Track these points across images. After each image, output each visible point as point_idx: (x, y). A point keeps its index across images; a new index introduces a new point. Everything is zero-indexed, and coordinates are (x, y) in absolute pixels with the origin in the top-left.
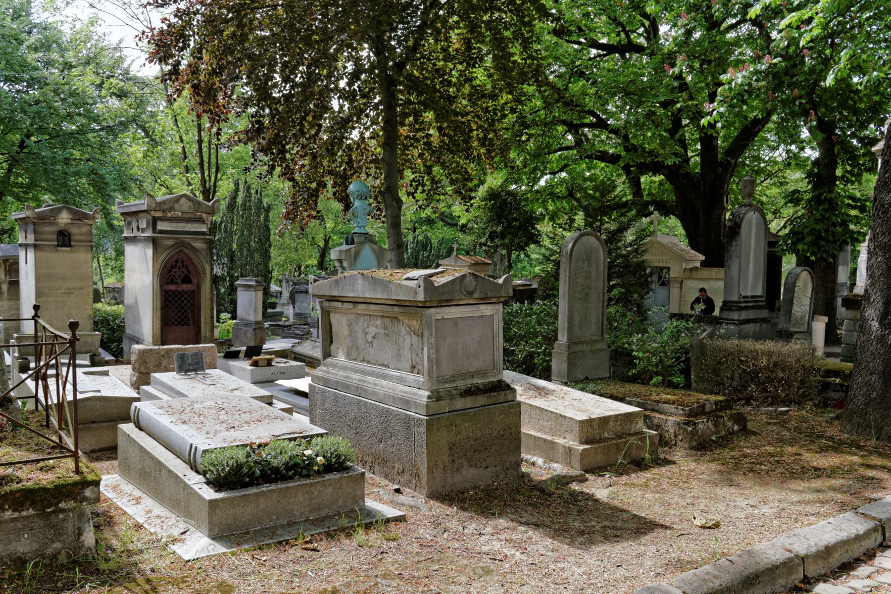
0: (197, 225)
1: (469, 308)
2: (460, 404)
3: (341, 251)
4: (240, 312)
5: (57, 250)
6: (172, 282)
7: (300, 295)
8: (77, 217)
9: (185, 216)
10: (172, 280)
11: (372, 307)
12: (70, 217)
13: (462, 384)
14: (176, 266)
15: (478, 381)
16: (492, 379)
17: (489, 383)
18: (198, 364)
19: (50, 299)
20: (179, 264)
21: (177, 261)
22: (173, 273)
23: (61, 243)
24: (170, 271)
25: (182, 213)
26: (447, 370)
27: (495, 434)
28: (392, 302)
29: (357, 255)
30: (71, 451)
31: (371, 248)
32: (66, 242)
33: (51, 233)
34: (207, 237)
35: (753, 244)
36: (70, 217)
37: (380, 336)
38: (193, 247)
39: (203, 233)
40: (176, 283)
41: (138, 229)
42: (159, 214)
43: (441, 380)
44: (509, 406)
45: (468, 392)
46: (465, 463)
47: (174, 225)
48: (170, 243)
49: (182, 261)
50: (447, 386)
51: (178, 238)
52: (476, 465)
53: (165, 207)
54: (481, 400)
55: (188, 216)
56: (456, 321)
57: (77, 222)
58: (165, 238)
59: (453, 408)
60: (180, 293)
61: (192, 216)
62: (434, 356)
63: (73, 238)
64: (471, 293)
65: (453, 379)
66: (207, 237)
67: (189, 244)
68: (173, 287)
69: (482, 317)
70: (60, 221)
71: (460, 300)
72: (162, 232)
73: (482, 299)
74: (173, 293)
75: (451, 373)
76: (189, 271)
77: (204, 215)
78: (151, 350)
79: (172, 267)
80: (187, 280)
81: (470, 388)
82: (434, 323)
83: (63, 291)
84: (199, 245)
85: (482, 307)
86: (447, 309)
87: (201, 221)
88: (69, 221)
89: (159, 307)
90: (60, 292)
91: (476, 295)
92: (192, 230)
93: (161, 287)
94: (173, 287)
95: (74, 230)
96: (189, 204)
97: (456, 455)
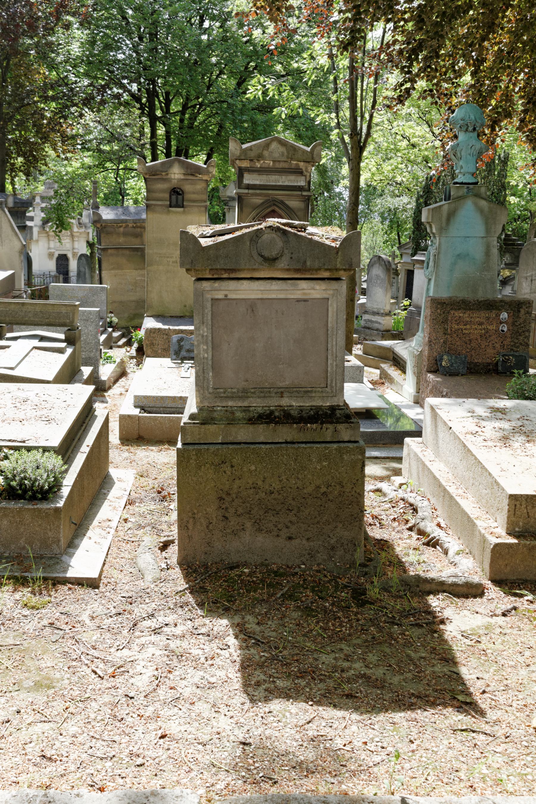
1: (275, 285)
2: (243, 433)
4: (414, 296)
5: (169, 212)
8: (189, 172)
9: (278, 165)
11: (249, 276)
12: (183, 171)
13: (258, 404)
15: (292, 403)
16: (318, 403)
17: (311, 408)
19: (161, 268)
23: (174, 202)
25: (274, 161)
26: (232, 379)
27: (310, 489)
29: (451, 215)
32: (180, 202)
33: (163, 191)
38: (287, 207)
42: (245, 164)
43: (220, 393)
44: (339, 450)
45: (267, 418)
46: (248, 525)
48: (258, 201)
50: (230, 403)
51: (268, 195)
52: (269, 532)
53: (252, 154)
54: (286, 432)
56: (252, 305)
57: (190, 177)
58: (253, 195)
59: (230, 439)
61: (285, 165)
63: (187, 196)
64: (271, 261)
65: (244, 394)
67: (282, 203)
69: (305, 300)
70: (172, 176)
71: (254, 270)
72: (249, 187)
75: (242, 384)
77: (302, 164)
78: (159, 330)
81: (272, 412)
82: (209, 305)
85: (303, 284)
86: (232, 285)
88: (182, 177)
90: (171, 260)
91: (283, 263)
92: (286, 183)
95: (187, 188)
96: (282, 149)
97: (232, 511)
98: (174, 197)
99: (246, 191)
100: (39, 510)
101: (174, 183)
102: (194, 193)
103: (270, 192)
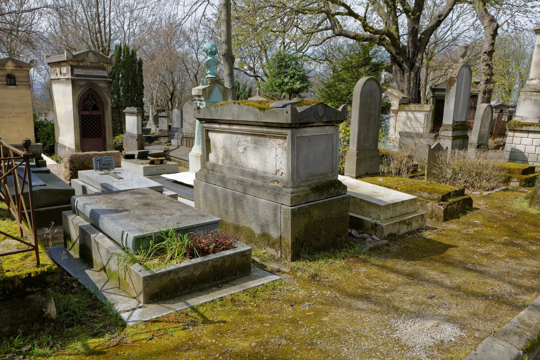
0: (100, 71)
1: (319, 129)
3: (199, 90)
6: (86, 109)
7: (162, 118)
9: (92, 65)
10: (86, 108)
12: (14, 65)
14: (88, 99)
18: (109, 164)
19: (5, 120)
20: (90, 97)
21: (88, 96)
22: (86, 103)
23: (9, 83)
24: (84, 102)
25: (90, 63)
28: (261, 124)
30: (32, 246)
31: (219, 87)
34: (108, 80)
35: (463, 88)
36: (14, 65)
37: (250, 148)
39: (105, 77)
40: (89, 110)
41: (61, 73)
42: (75, 64)
47: (85, 71)
48: (83, 83)
49: (92, 96)
53: (80, 59)
55: (95, 65)
56: (309, 138)
59: (308, 201)
60: (91, 116)
61: (97, 65)
62: (295, 164)
66: (108, 80)
68: (86, 113)
69: (326, 135)
70: (7, 68)
71: (314, 123)
73: (327, 122)
74: (87, 116)
76: (96, 102)
77: (105, 65)
79: (85, 100)
80: (95, 108)
83: (13, 115)
84: (102, 85)
85: (327, 128)
87: (104, 69)
88: (14, 68)
89: (78, 126)
92: (98, 74)
93: (79, 112)
94: (86, 113)
95: (17, 74)
98: (9, 80)
99: (76, 78)
100: (254, 293)
101: (8, 72)
102: (22, 78)
103: (90, 78)
